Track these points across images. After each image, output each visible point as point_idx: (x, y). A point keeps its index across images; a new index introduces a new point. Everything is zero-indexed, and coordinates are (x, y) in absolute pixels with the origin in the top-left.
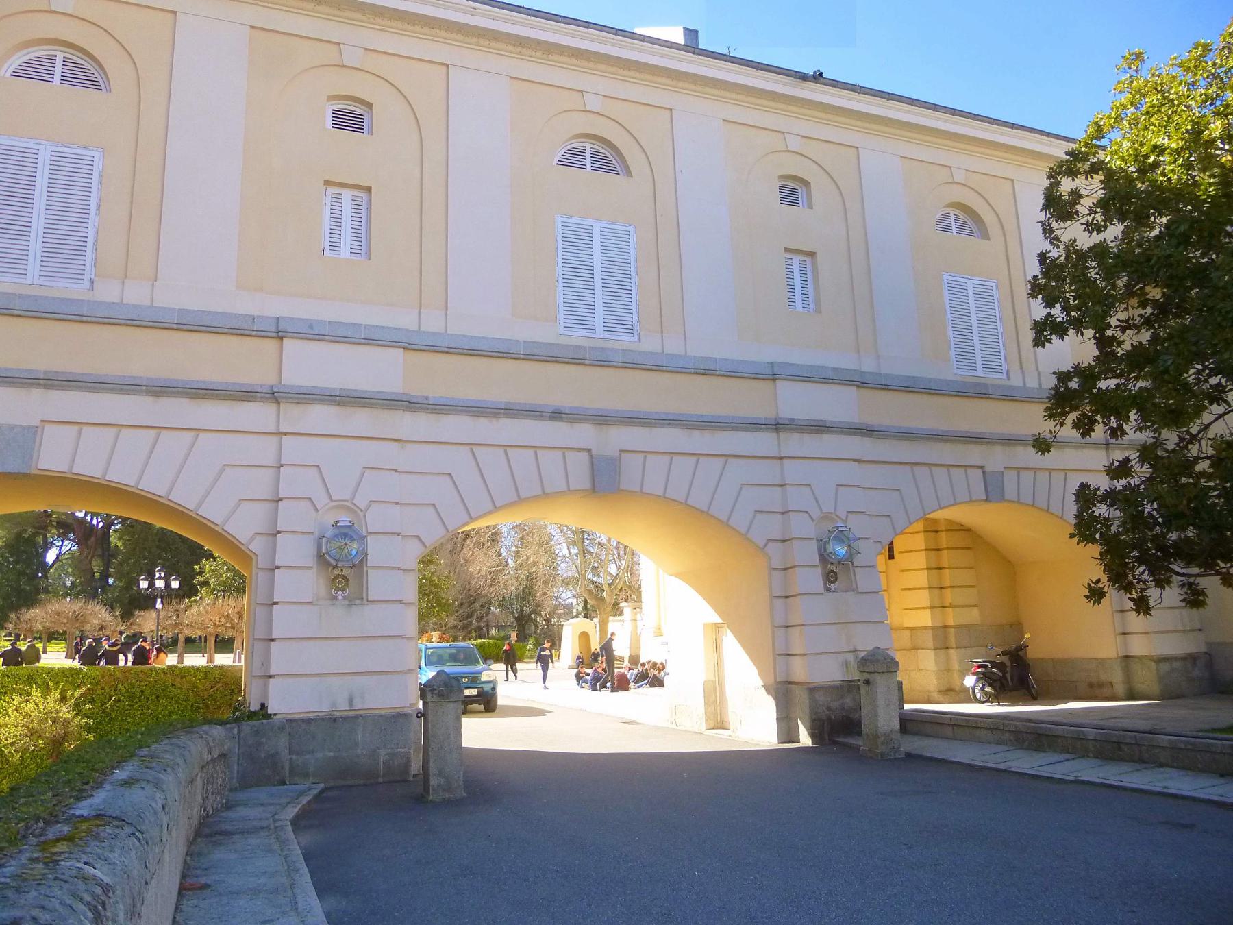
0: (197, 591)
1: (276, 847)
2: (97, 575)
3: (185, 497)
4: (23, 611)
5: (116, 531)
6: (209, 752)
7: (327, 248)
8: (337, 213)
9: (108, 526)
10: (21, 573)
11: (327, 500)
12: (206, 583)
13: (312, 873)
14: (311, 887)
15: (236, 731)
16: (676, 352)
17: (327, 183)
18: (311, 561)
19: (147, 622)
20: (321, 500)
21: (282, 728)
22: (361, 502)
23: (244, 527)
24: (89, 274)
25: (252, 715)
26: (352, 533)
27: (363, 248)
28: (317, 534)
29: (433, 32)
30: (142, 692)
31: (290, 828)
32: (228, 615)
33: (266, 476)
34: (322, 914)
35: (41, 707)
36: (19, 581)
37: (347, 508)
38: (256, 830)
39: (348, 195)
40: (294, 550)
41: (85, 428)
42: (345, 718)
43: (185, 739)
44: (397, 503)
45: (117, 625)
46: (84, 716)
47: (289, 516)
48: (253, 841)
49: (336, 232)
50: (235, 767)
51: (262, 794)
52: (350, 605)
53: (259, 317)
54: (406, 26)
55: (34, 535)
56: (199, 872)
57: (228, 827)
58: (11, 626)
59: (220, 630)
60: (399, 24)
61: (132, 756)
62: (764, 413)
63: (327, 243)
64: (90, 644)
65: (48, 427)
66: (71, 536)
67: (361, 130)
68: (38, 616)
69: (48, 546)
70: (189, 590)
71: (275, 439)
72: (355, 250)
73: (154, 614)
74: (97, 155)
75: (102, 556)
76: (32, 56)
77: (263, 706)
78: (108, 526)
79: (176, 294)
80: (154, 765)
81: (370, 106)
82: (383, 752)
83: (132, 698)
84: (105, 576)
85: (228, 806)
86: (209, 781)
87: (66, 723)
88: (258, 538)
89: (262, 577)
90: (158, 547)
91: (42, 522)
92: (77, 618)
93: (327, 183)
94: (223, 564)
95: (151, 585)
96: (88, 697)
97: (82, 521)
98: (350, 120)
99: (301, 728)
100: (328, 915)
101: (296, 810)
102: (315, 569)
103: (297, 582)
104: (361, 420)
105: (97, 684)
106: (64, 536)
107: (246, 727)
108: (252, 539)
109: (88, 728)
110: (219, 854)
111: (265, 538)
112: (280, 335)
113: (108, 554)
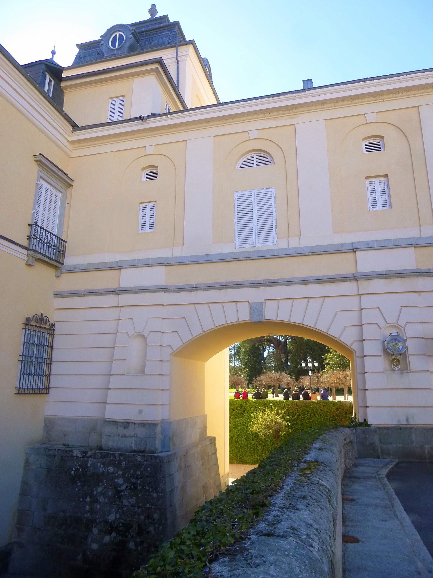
1: (381, 486)
2: (283, 361)
3: (322, 327)
4: (258, 377)
5: (289, 342)
6: (345, 440)
7: (371, 207)
8: (373, 191)
9: (286, 340)
10: (255, 361)
11: (385, 324)
12: (328, 364)
13: (401, 501)
14: (402, 508)
15: (354, 431)
16: (284, 247)
17: (367, 178)
18: (380, 352)
19: (306, 381)
20: (382, 323)
21: (375, 431)
22: (402, 322)
23: (348, 338)
24: (275, 238)
25: (361, 424)
26: (399, 339)
27: (388, 203)
28: (382, 340)
29: (408, 93)
30: (308, 412)
31: (386, 479)
33: (356, 313)
34: (410, 522)
35: (270, 417)
36: (255, 364)
37: (395, 327)
38: (370, 478)
39: (377, 181)
40: (372, 348)
41: (280, 301)
42: (405, 428)
43: (335, 433)
44: (420, 323)
45: (294, 383)
46: (287, 421)
47: (369, 332)
48: (370, 483)
49: (374, 199)
50: (356, 447)
51: (369, 461)
52: (402, 373)
53: (344, 244)
54: (395, 96)
55: (259, 345)
56: (348, 493)
57: (357, 475)
58: (254, 383)
60: (391, 96)
61: (317, 438)
62: (349, 270)
63: (370, 205)
64: (286, 391)
65: (267, 302)
66: (272, 345)
67: (379, 149)
68: (263, 379)
69: (264, 350)
70: (322, 367)
71: (357, 298)
72: (384, 205)
73: (308, 378)
74: (273, 190)
75: (284, 353)
76: (248, 157)
77: (365, 420)
78: (286, 340)
79: (309, 240)
80: (327, 443)
81: (382, 137)
82: (427, 447)
83: (304, 414)
84: (287, 361)
85: (355, 465)
86: (346, 453)
87: (280, 424)
88: (355, 343)
89: (358, 360)
90: (307, 348)
91: (261, 341)
92: (278, 380)
93: (367, 178)
94: (335, 355)
95: (307, 365)
96: (287, 413)
97: (276, 339)
98: (374, 146)
99: (384, 431)
100: (413, 522)
101: (387, 471)
102: (383, 357)
103: (375, 363)
104: (396, 284)
105: (290, 408)
106: (270, 345)
107: (359, 429)
108: (352, 344)
109: (288, 426)
110: (356, 487)
111: (357, 343)
112: (354, 250)
113: (287, 352)
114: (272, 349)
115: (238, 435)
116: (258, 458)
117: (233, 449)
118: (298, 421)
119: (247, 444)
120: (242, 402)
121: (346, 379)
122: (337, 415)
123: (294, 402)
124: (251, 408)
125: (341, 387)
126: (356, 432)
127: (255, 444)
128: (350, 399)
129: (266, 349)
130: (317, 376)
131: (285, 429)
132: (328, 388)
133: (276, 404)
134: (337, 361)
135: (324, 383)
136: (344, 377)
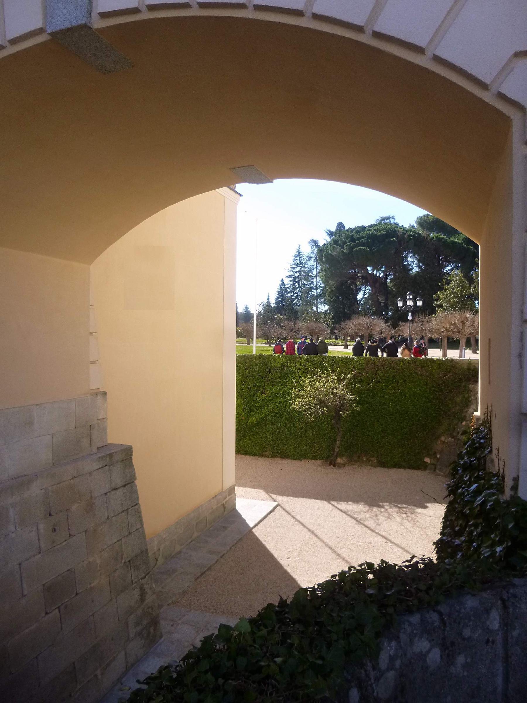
0: (436, 311)
12: (440, 306)
30: (394, 376)
32: (455, 323)
36: (344, 309)
45: (390, 331)
59: (449, 333)
70: (429, 309)
95: (405, 303)
105: (364, 369)
114: (368, 289)
115: (277, 413)
116: (306, 450)
117: (268, 434)
118: (375, 391)
119: (291, 427)
120: (284, 360)
121: (464, 324)
122: (444, 382)
123: (371, 360)
124: (299, 369)
125: (456, 336)
126: (506, 625)
127: (302, 428)
128: (469, 355)
129: (360, 290)
130: (423, 322)
131: (351, 406)
132: (438, 338)
133: (341, 362)
134: (454, 302)
135: (431, 331)
136: (462, 322)
